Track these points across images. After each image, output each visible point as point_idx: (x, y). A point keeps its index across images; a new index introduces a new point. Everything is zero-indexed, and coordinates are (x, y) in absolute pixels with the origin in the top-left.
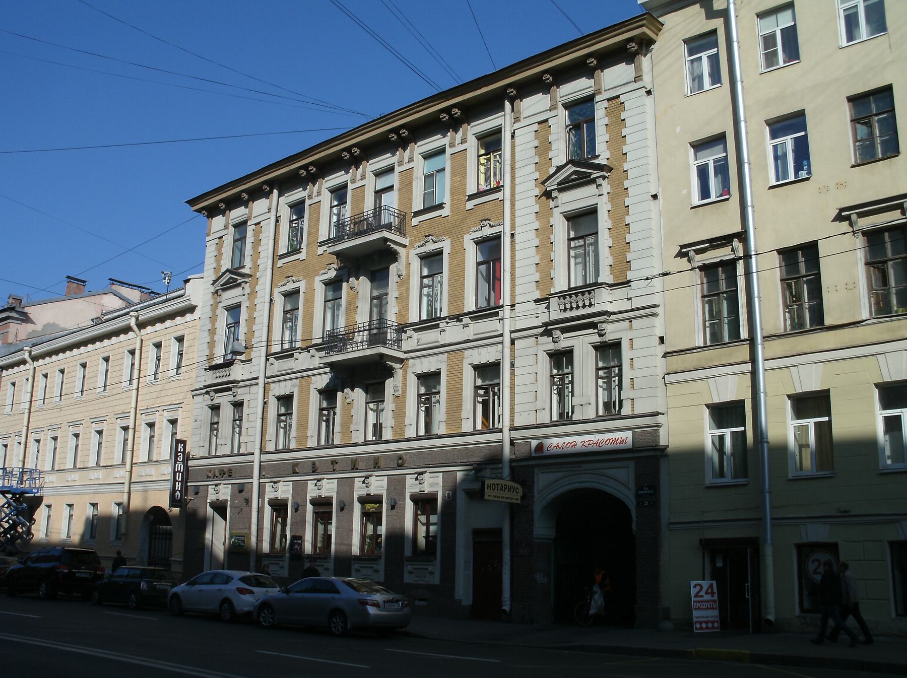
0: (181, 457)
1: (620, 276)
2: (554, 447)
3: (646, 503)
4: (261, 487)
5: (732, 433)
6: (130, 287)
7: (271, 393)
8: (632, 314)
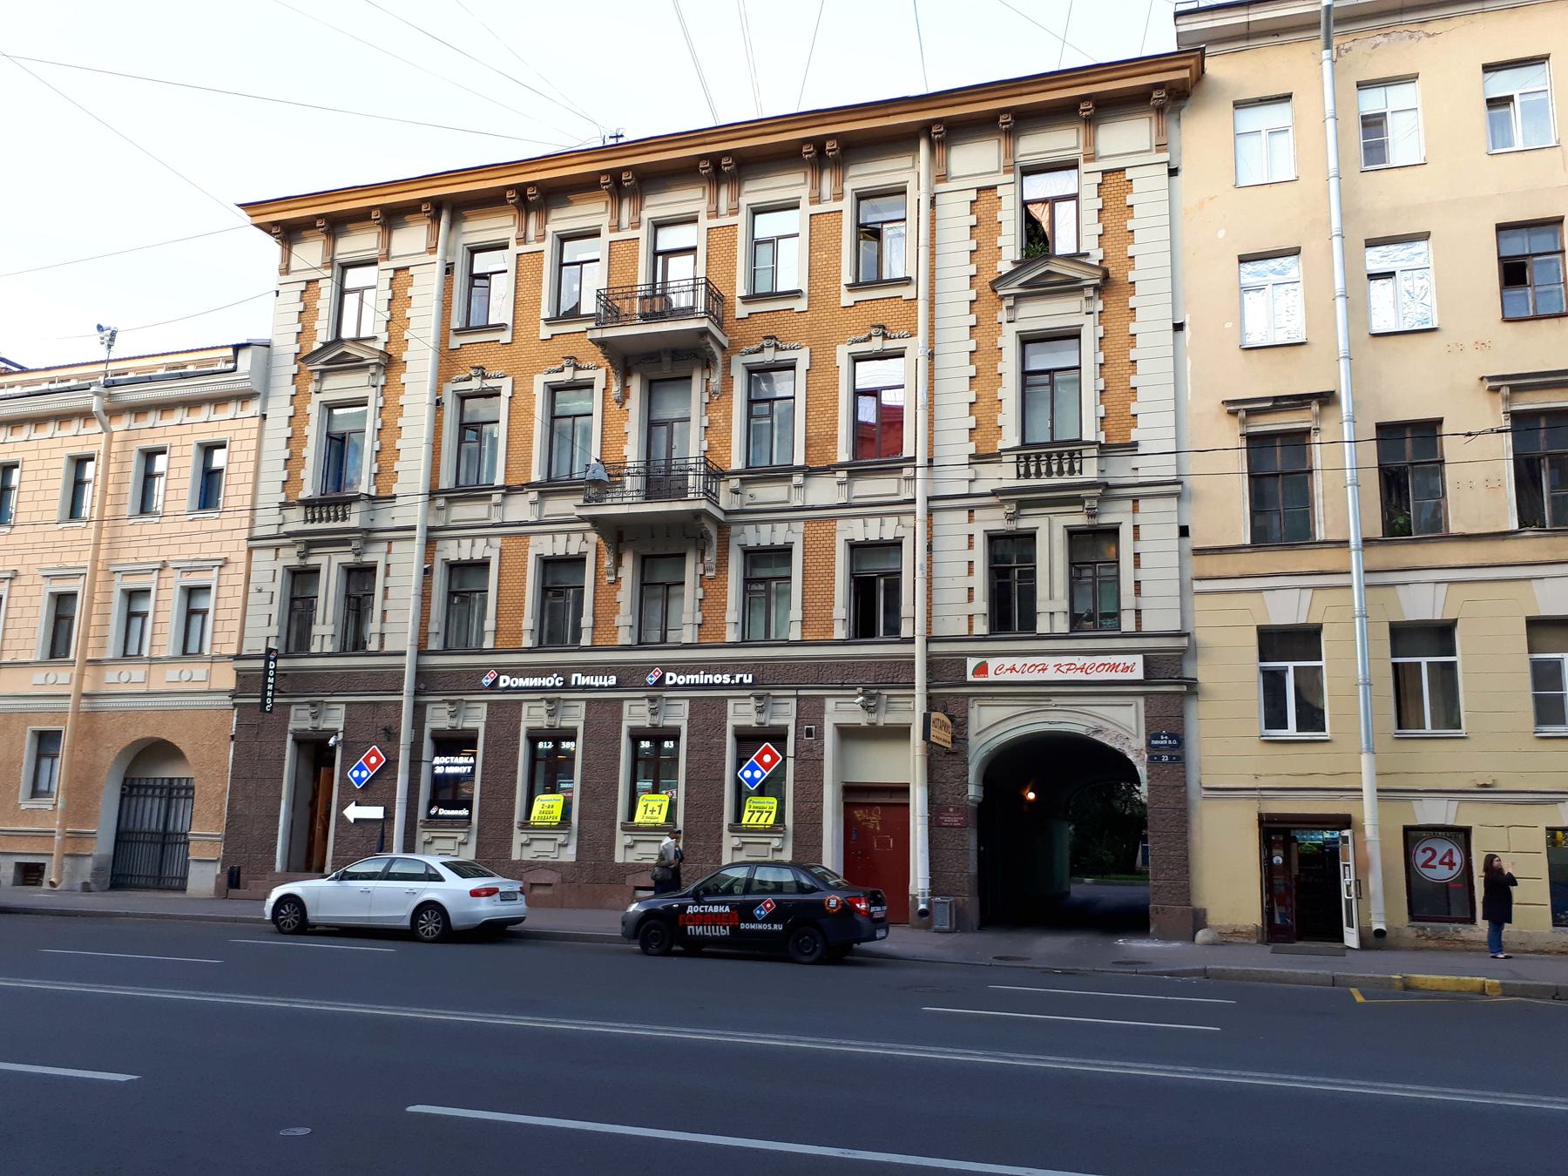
2: (1007, 670)
3: (1165, 758)
4: (419, 710)
7: (438, 557)
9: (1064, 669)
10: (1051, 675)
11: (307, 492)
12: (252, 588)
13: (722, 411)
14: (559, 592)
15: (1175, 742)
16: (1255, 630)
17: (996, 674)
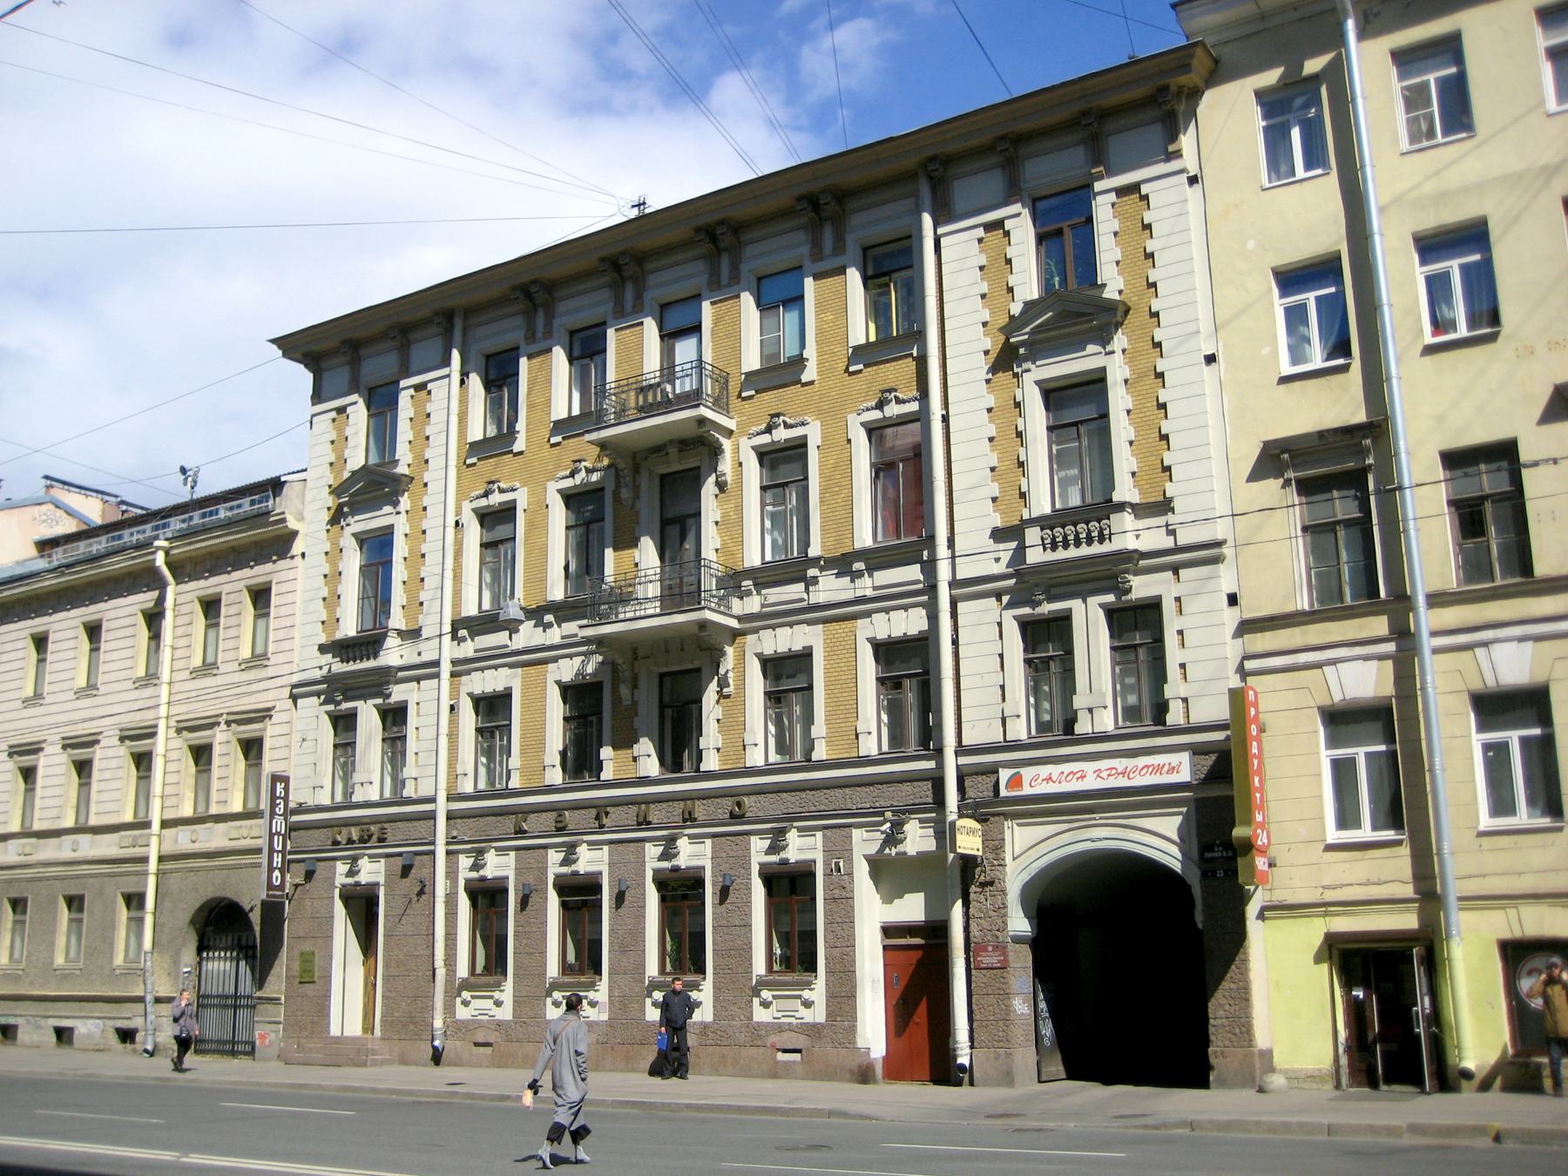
0: (282, 806)
1: (1151, 490)
5: (1367, 754)
6: (83, 492)
7: (464, 690)
8: (1177, 560)
9: (1104, 774)
10: (1091, 783)
14: (589, 724)
15: (1230, 854)
17: (1031, 786)
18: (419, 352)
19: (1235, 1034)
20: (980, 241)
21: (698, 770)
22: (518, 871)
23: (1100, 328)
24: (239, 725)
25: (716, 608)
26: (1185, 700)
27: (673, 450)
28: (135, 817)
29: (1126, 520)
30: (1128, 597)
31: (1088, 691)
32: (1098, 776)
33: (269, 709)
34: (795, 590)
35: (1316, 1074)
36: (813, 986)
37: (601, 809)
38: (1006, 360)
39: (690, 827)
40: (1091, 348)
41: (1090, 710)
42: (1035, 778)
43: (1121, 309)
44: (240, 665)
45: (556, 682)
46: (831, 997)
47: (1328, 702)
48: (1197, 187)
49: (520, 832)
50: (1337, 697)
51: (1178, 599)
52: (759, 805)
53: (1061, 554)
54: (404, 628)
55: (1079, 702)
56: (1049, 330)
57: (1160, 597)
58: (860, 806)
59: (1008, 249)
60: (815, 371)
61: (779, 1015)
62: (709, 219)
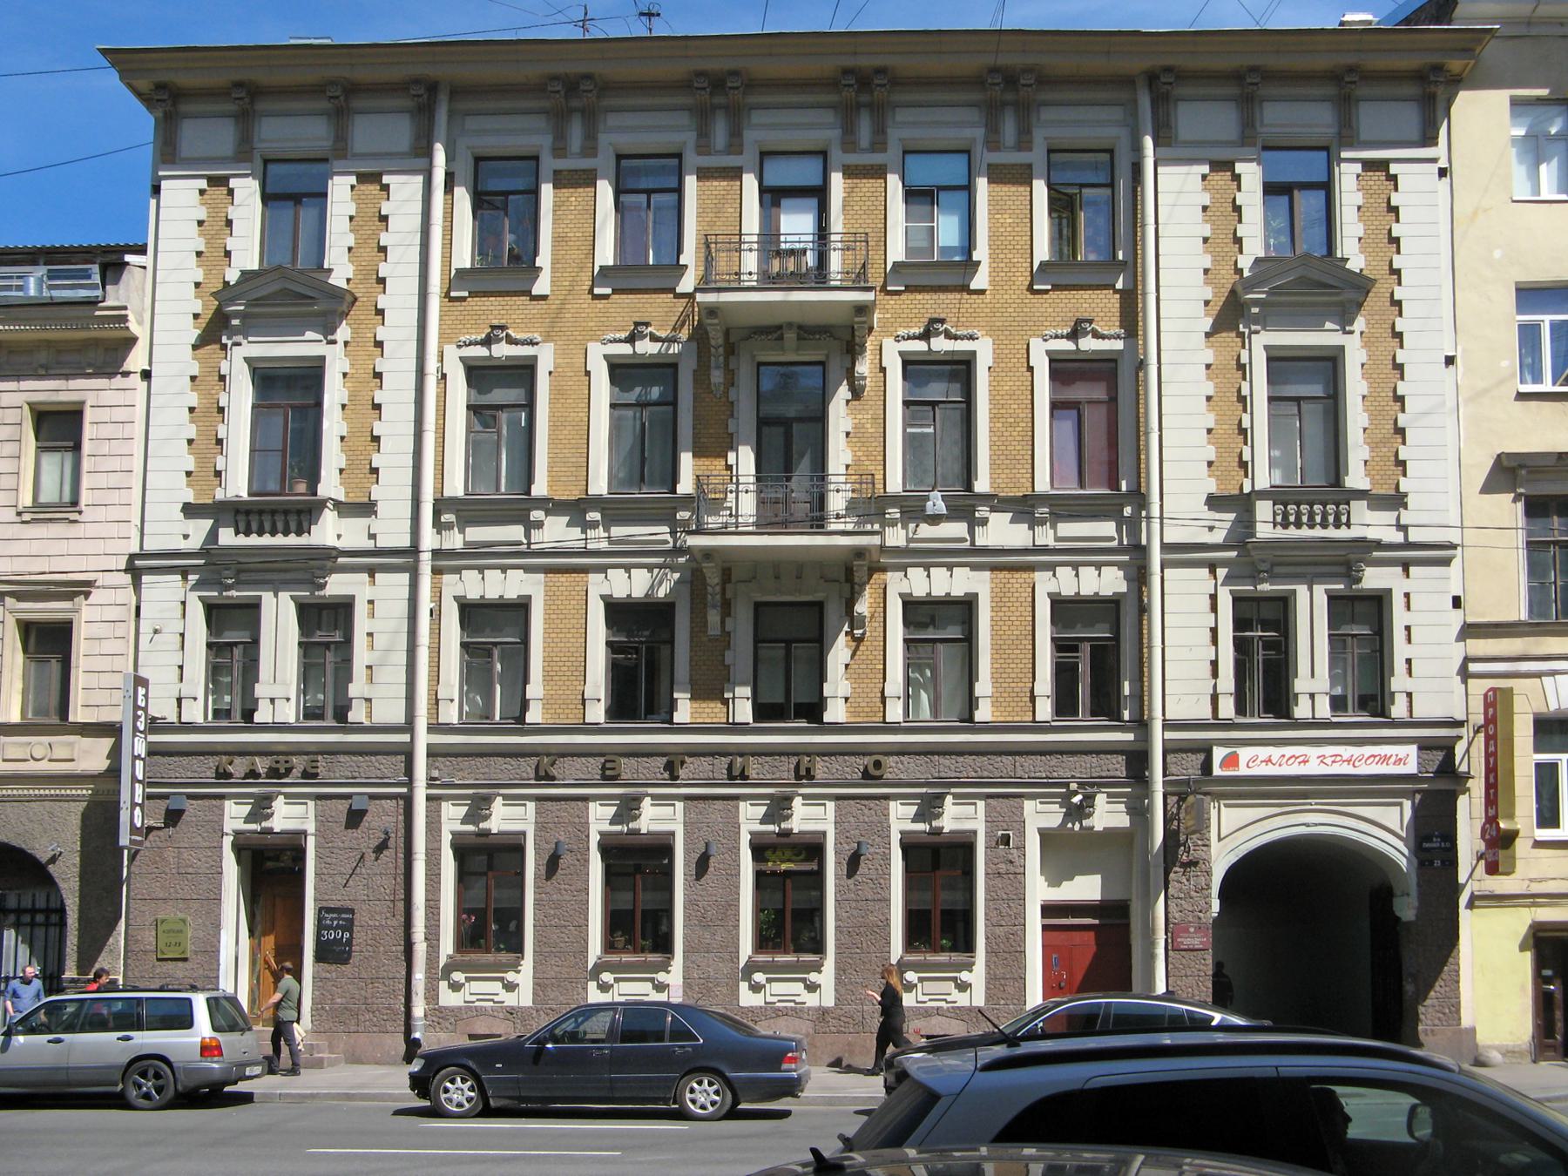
2: (1262, 762)
3: (1437, 863)
9: (1328, 761)
10: (1313, 768)
11: (237, 486)
12: (146, 627)
13: (870, 412)
16: (1531, 717)
18: (1369, 116)
19: (1444, 1014)
20: (202, 192)
21: (971, 719)
22: (541, 827)
23: (324, 314)
24: (18, 601)
25: (856, 529)
26: (1409, 695)
27: (790, 336)
28: (22, 719)
29: (1359, 509)
30: (322, 593)
31: (272, 681)
32: (1322, 761)
33: (90, 584)
34: (515, 532)
35: (1516, 1049)
36: (519, 968)
37: (673, 762)
38: (214, 331)
39: (803, 786)
40: (310, 335)
41: (272, 700)
42: (1254, 759)
43: (349, 298)
44: (19, 514)
45: (455, 598)
46: (992, 979)
47: (1543, 710)
48: (1446, 180)
49: (545, 777)
50: (1553, 706)
51: (371, 602)
52: (901, 766)
53: (1293, 532)
54: (342, 499)
55: (260, 690)
56: (1280, 294)
57: (353, 597)
58: (1033, 775)
59: (230, 209)
60: (987, 279)
61: (926, 998)
62: (865, 62)
